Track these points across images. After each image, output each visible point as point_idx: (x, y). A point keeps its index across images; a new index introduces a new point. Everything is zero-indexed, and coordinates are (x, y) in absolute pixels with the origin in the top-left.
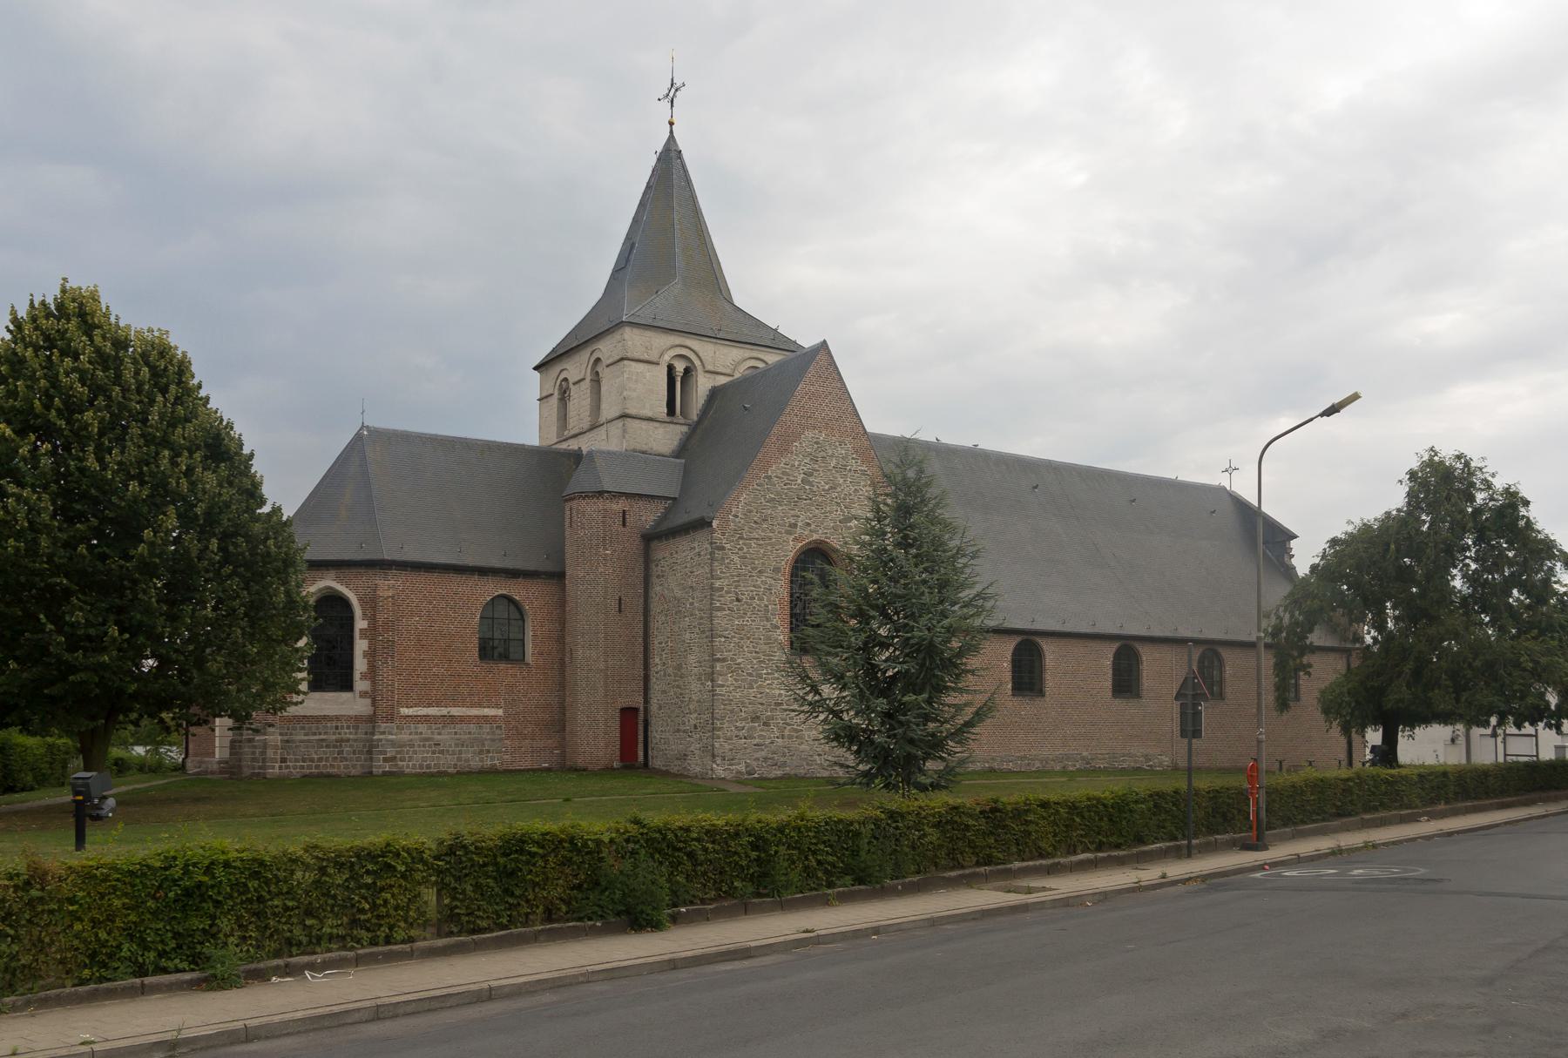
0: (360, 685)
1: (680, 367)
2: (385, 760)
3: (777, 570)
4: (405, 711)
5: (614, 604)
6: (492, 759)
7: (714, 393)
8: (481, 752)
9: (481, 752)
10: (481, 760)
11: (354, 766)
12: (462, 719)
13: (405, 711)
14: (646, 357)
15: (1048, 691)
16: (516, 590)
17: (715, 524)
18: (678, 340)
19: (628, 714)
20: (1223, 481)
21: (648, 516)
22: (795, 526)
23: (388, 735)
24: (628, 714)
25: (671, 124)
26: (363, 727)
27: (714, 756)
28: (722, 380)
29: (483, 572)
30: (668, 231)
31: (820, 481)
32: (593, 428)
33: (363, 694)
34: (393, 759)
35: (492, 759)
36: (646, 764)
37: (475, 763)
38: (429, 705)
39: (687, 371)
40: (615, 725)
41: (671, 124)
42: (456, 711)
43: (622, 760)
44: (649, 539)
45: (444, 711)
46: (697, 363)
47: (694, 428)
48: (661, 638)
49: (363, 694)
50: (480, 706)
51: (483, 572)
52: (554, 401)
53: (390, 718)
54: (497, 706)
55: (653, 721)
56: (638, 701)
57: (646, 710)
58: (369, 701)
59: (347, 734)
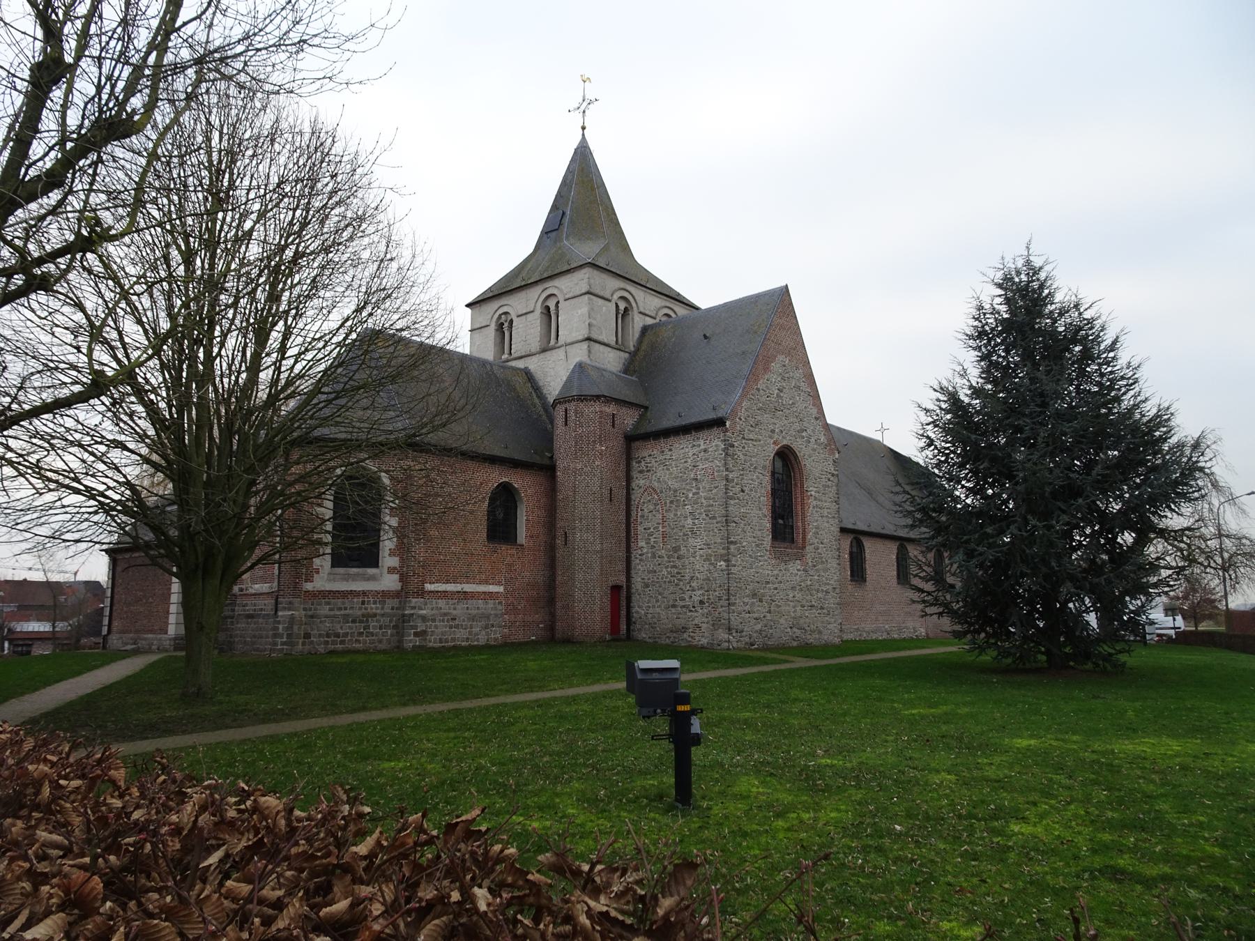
0: (388, 560)
1: (622, 306)
2: (416, 634)
3: (764, 467)
4: (429, 587)
5: (607, 493)
6: (495, 632)
7: (645, 330)
8: (486, 627)
9: (486, 627)
10: (487, 634)
11: (380, 641)
12: (465, 595)
13: (429, 587)
14: (601, 294)
15: (869, 578)
16: (518, 481)
17: (728, 424)
18: (622, 284)
19: (616, 589)
20: (877, 436)
21: (629, 419)
22: (773, 431)
23: (421, 608)
24: (616, 589)
25: (583, 128)
26: (395, 602)
27: (730, 629)
28: (649, 321)
29: (492, 460)
30: (582, 205)
31: (786, 400)
32: (544, 350)
33: (391, 570)
34: (424, 633)
35: (495, 632)
36: (629, 637)
37: (482, 639)
38: (448, 582)
39: (626, 309)
40: (607, 601)
41: (583, 128)
42: (468, 588)
43: (611, 634)
44: (632, 439)
45: (458, 587)
46: (634, 304)
47: (633, 355)
48: (647, 525)
49: (391, 570)
50: (487, 582)
51: (492, 460)
52: (491, 332)
53: (422, 593)
54: (499, 583)
55: (635, 598)
56: (622, 580)
57: (629, 587)
58: (396, 577)
59: (373, 608)
